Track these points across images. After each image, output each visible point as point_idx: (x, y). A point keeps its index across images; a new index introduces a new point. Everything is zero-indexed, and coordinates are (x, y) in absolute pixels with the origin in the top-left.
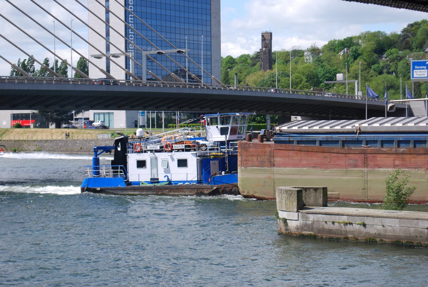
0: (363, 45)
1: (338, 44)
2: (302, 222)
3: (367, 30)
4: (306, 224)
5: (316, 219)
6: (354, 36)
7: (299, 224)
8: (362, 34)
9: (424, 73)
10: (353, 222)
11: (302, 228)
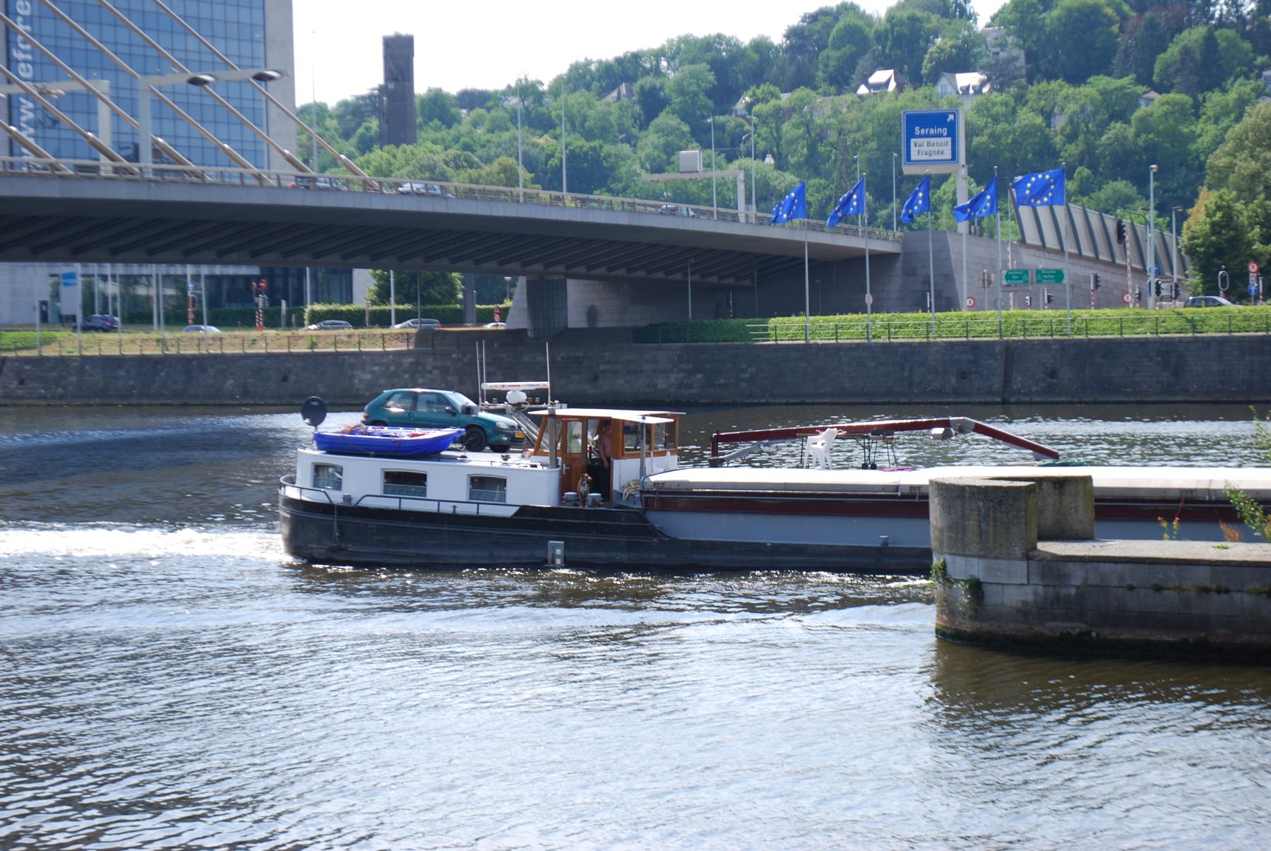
0: (672, 75)
1: (598, 70)
2: (1040, 589)
3: (682, 33)
4: (1057, 596)
5: (1093, 580)
6: (645, 48)
7: (1030, 598)
8: (670, 41)
9: (941, 149)
10: (1231, 587)
11: (1042, 610)
